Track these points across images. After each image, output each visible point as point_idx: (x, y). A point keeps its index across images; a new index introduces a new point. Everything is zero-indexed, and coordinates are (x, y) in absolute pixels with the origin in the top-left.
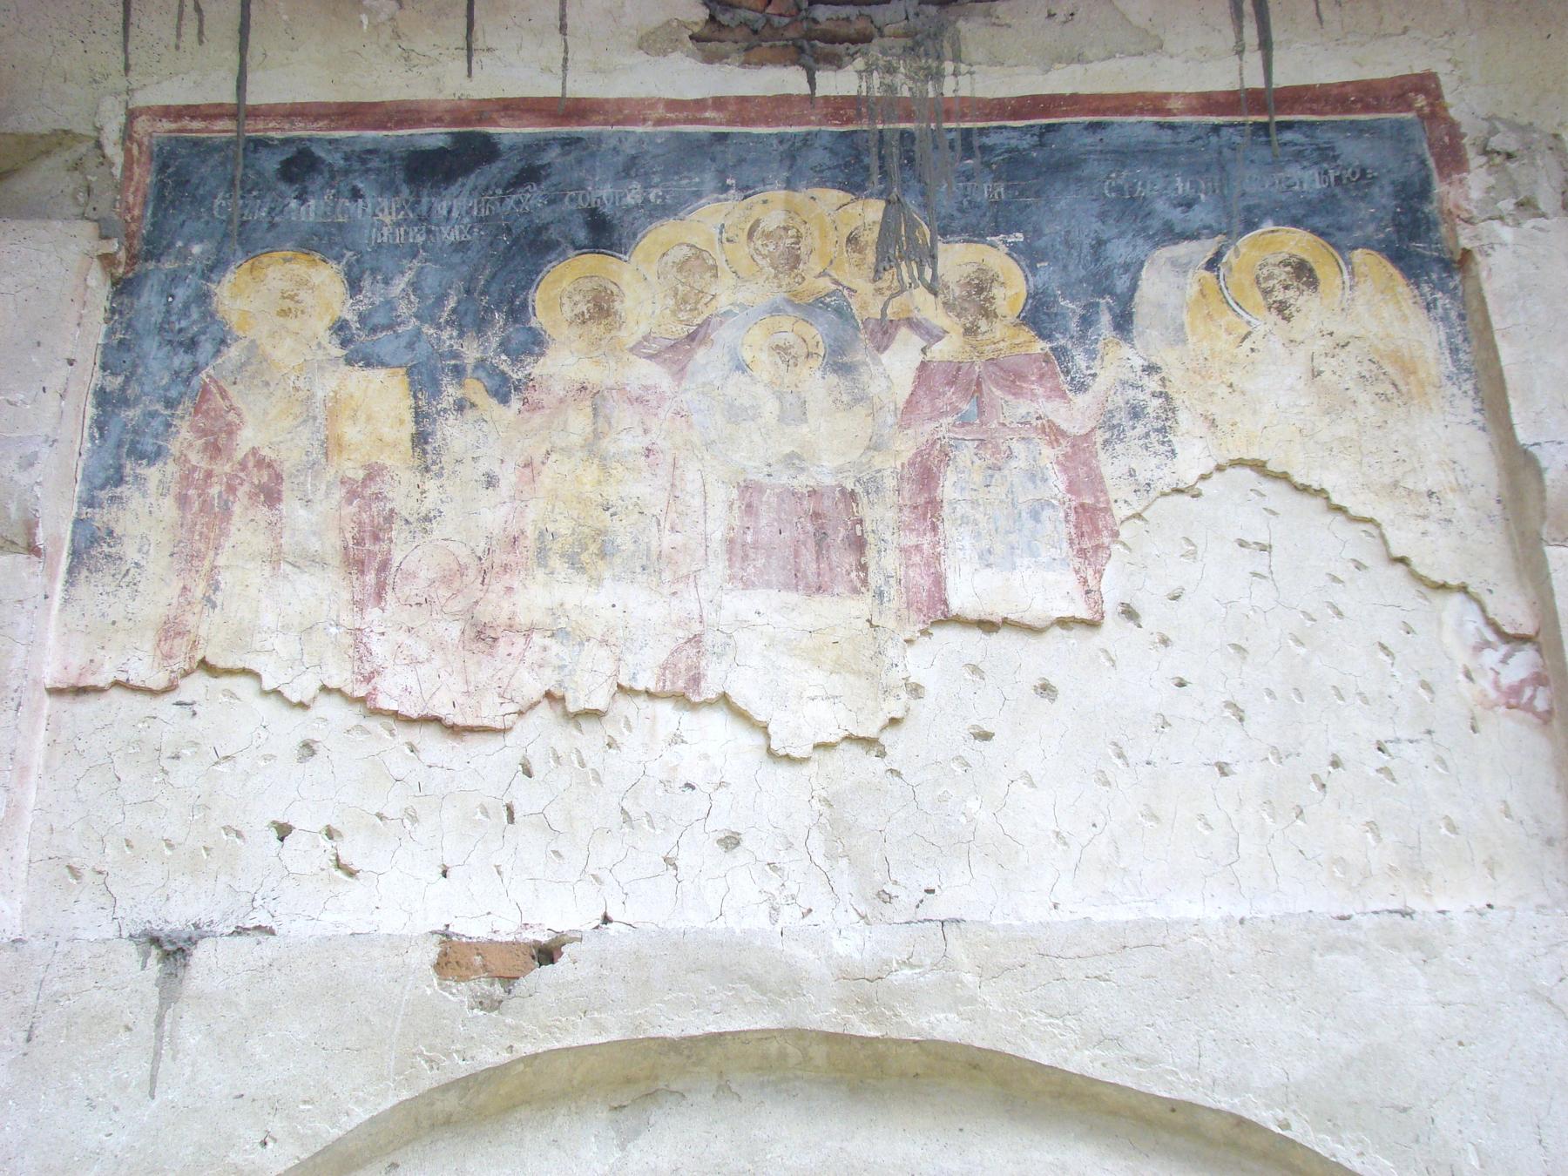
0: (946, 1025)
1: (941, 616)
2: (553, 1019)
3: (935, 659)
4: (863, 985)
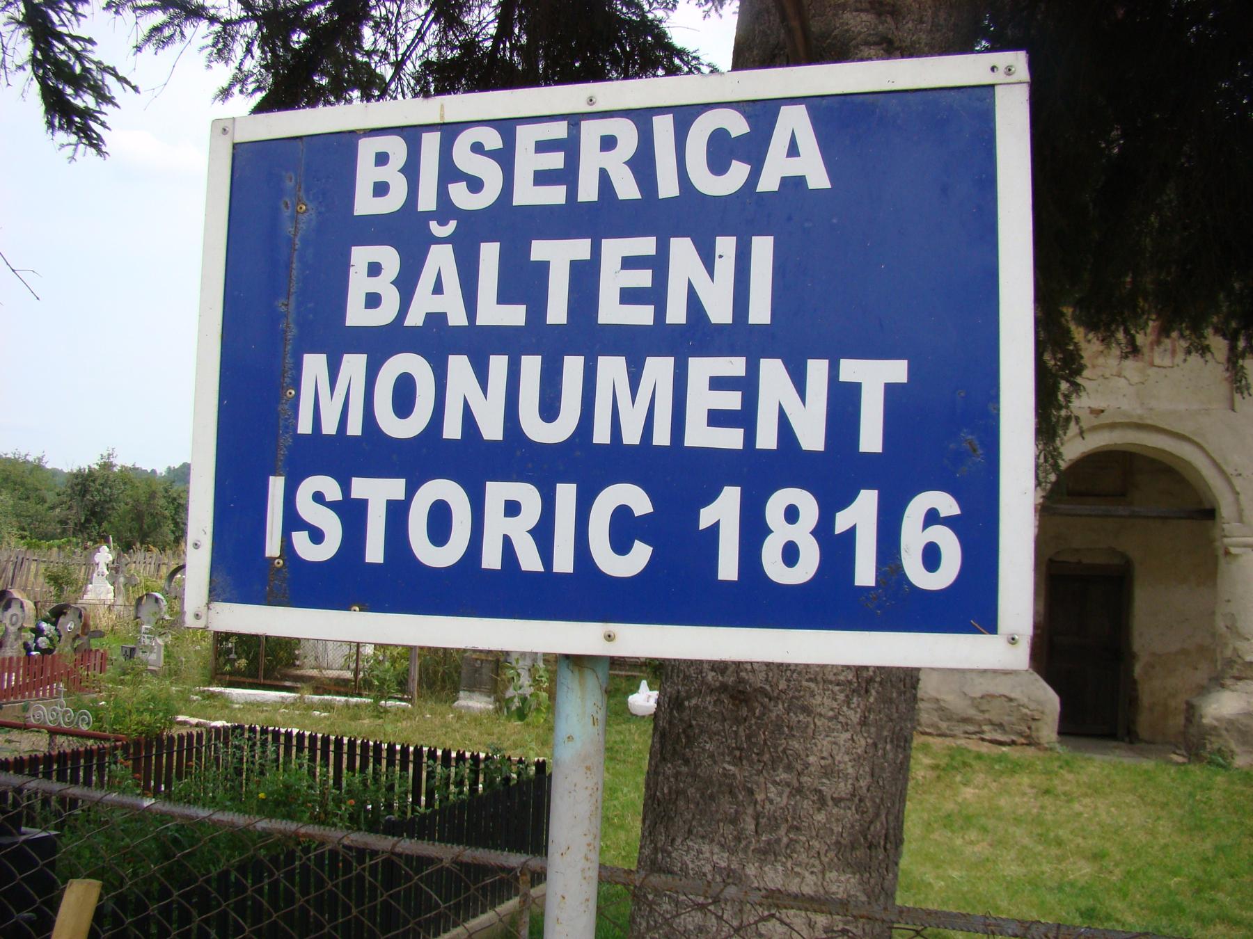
0: (1149, 422)
1: (1152, 365)
2: (1103, 419)
3: (1151, 372)
4: (1140, 417)
